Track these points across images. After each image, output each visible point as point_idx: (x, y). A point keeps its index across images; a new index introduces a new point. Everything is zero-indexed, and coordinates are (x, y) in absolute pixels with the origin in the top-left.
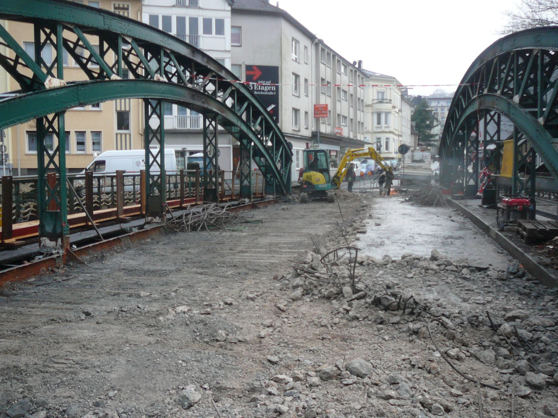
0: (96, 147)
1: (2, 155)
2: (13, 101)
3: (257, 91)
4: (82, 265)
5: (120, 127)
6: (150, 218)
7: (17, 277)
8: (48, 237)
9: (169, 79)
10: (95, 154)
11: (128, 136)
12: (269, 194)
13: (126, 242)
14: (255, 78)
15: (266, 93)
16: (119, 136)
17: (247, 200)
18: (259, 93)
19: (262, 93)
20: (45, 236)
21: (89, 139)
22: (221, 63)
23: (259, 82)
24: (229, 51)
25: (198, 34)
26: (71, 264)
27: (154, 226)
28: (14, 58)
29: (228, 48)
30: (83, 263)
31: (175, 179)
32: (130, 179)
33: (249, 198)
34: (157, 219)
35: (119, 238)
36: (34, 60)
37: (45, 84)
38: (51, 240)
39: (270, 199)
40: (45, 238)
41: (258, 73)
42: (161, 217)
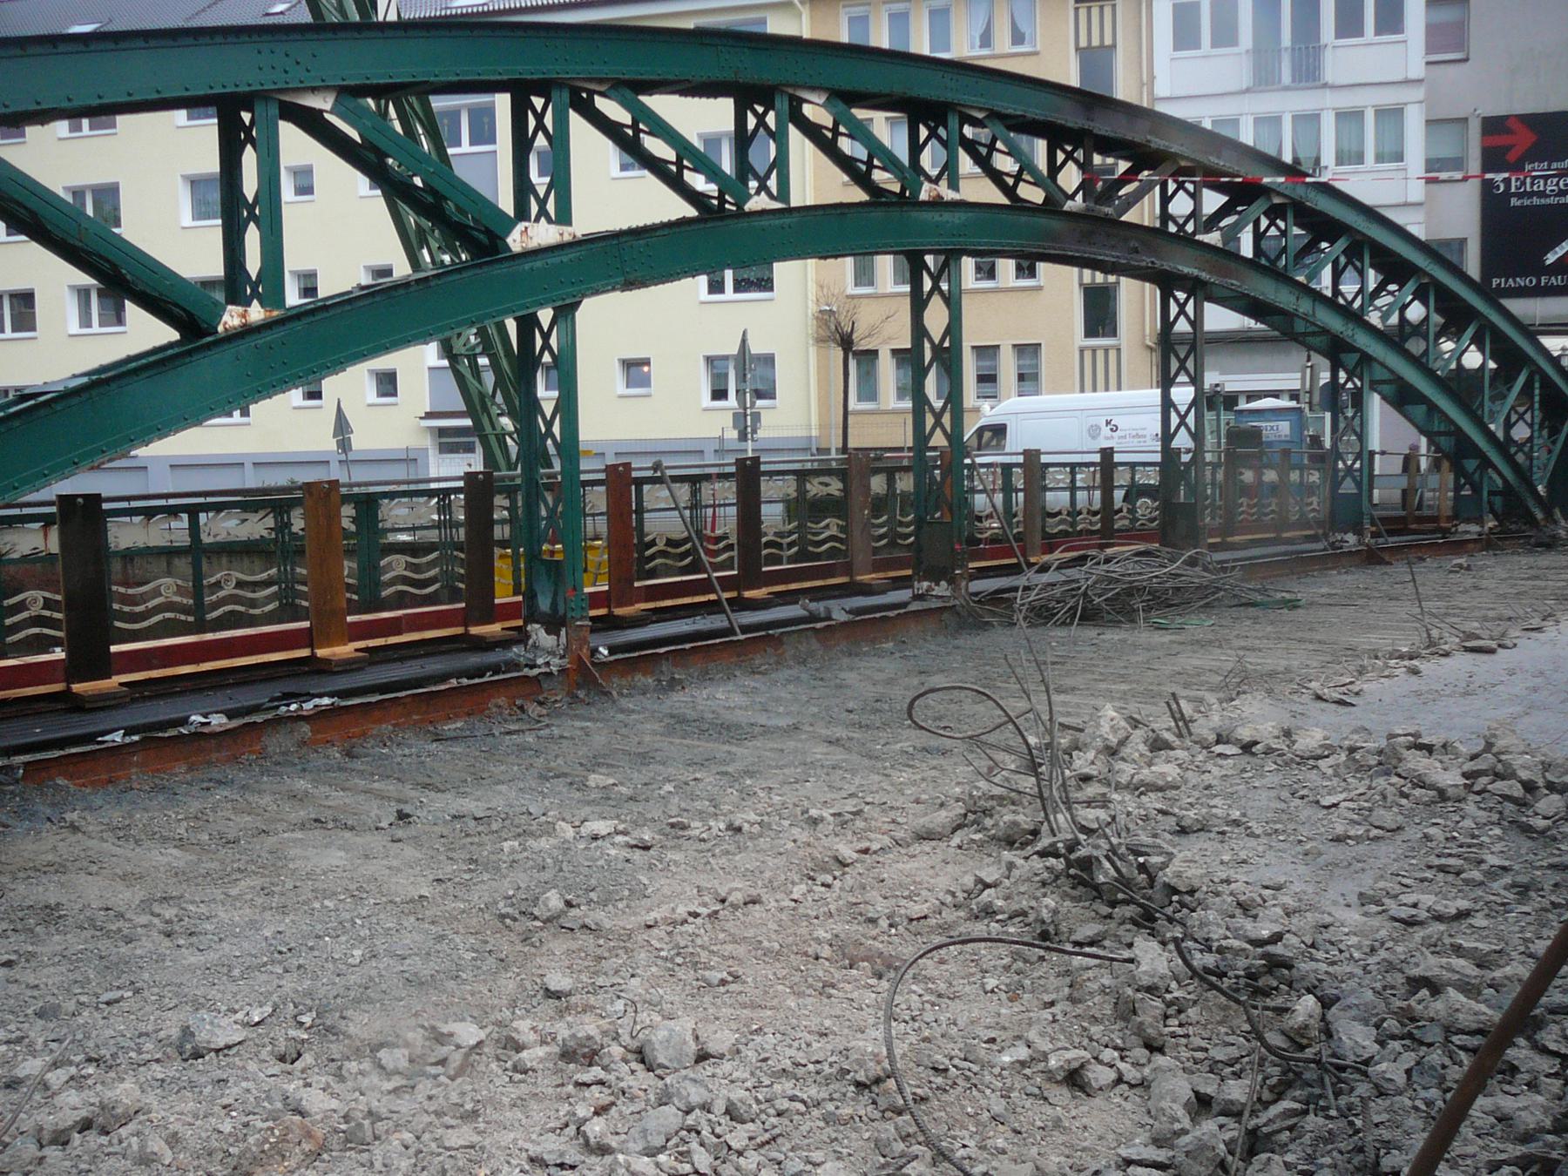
0: (988, 388)
1: (745, 415)
2: (402, 291)
3: (1520, 196)
4: (604, 698)
5: (1090, 332)
6: (925, 584)
7: (415, 717)
8: (542, 624)
9: (1010, 192)
10: (986, 406)
11: (1112, 354)
12: (1468, 521)
13: (803, 648)
14: (1511, 157)
15: (1551, 201)
16: (1088, 355)
17: (1351, 538)
18: (1527, 202)
19: (1536, 201)
20: (537, 622)
21: (1008, 367)
22: (629, 159)
23: (1528, 167)
24: (1420, 81)
25: (1319, 39)
26: (581, 694)
27: (934, 604)
28: (865, 159)
29: (1417, 69)
30: (608, 694)
31: (1128, 476)
32: (1062, 477)
33: (1359, 532)
34: (942, 589)
35: (769, 635)
36: (907, 164)
37: (509, 240)
38: (548, 632)
39: (1468, 537)
40: (537, 626)
41: (1524, 139)
42: (952, 581)
